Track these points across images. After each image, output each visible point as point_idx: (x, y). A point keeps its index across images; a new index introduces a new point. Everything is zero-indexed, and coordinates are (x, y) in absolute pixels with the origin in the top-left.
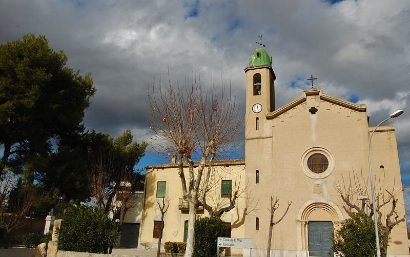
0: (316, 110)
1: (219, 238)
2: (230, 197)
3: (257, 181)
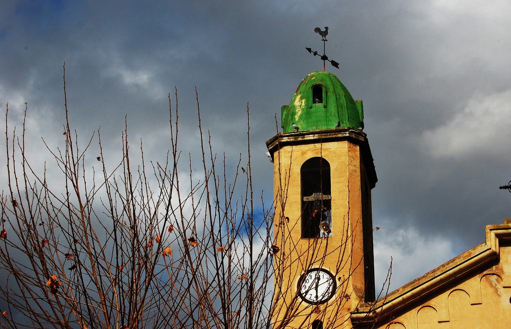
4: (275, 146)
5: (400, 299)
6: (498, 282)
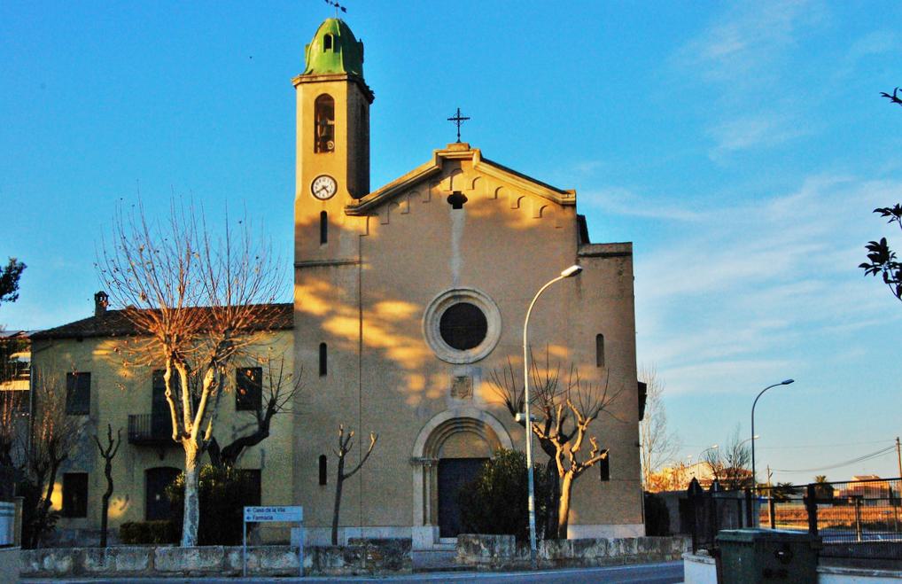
1: (246, 508)
2: (258, 406)
3: (323, 371)
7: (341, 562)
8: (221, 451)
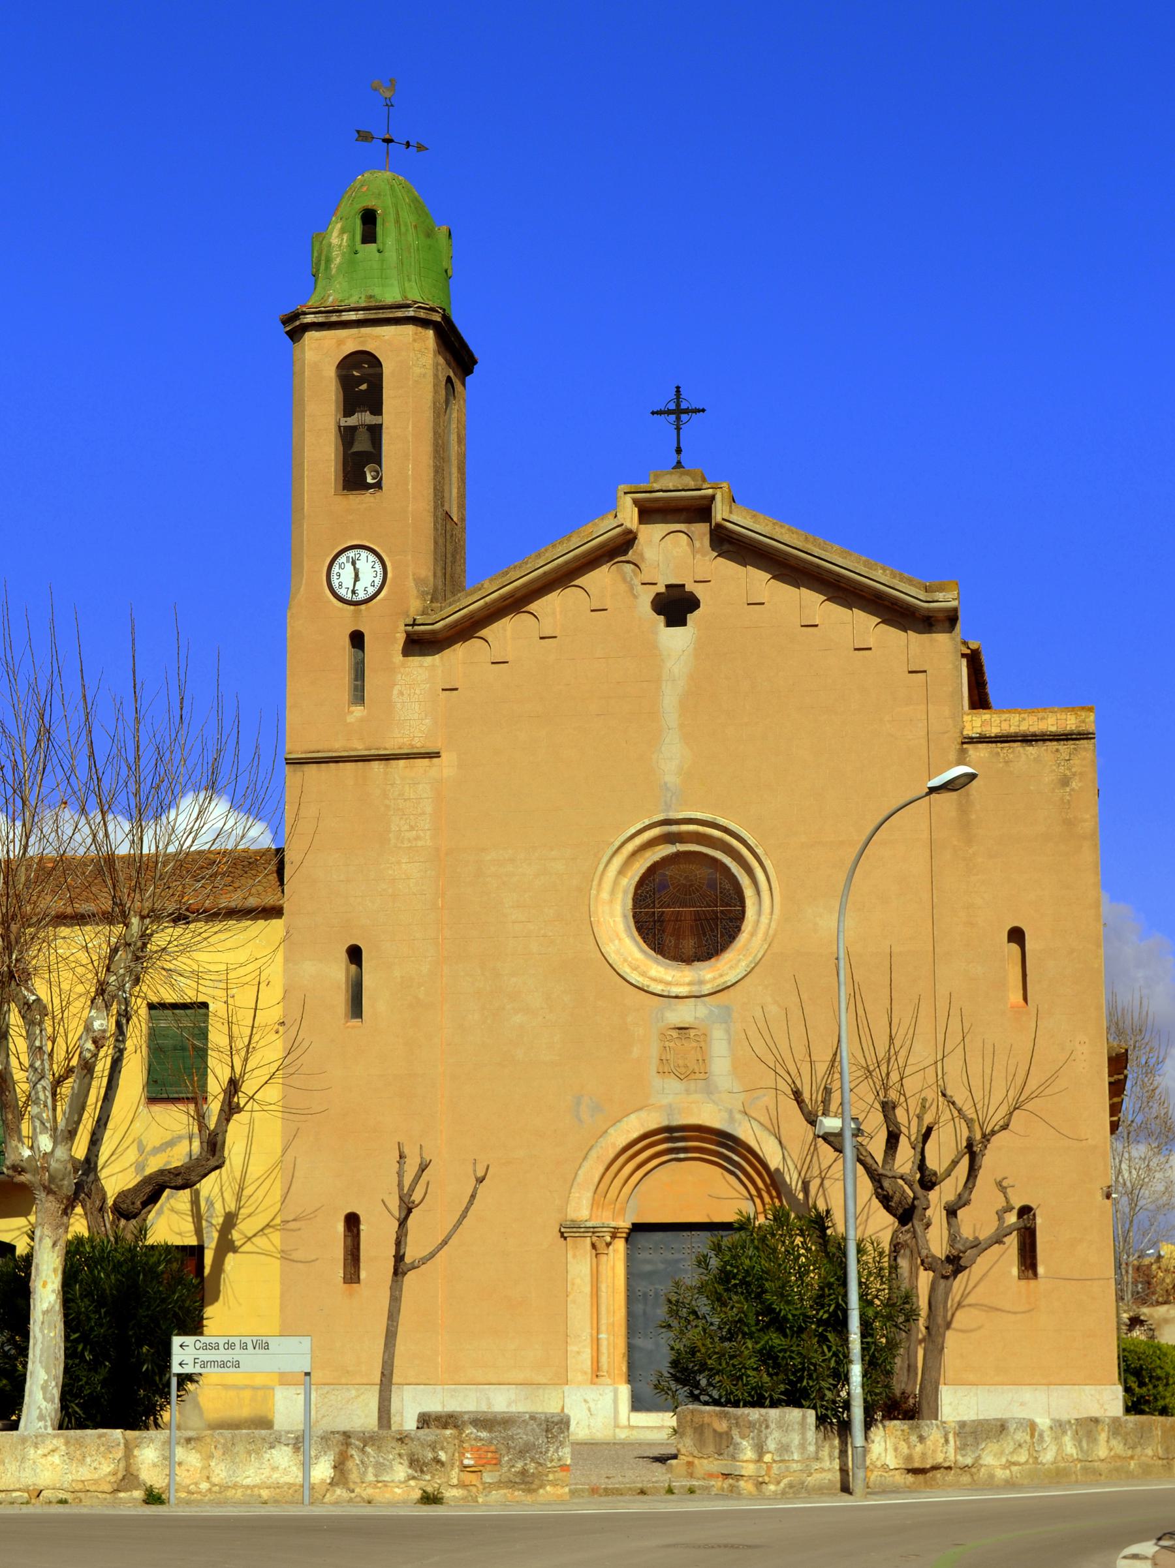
0: (692, 603)
1: (177, 1341)
2: (198, 1098)
3: (356, 1006)
4: (296, 329)
5: (481, 603)
6: (635, 575)
7: (401, 1471)
8: (110, 1202)
